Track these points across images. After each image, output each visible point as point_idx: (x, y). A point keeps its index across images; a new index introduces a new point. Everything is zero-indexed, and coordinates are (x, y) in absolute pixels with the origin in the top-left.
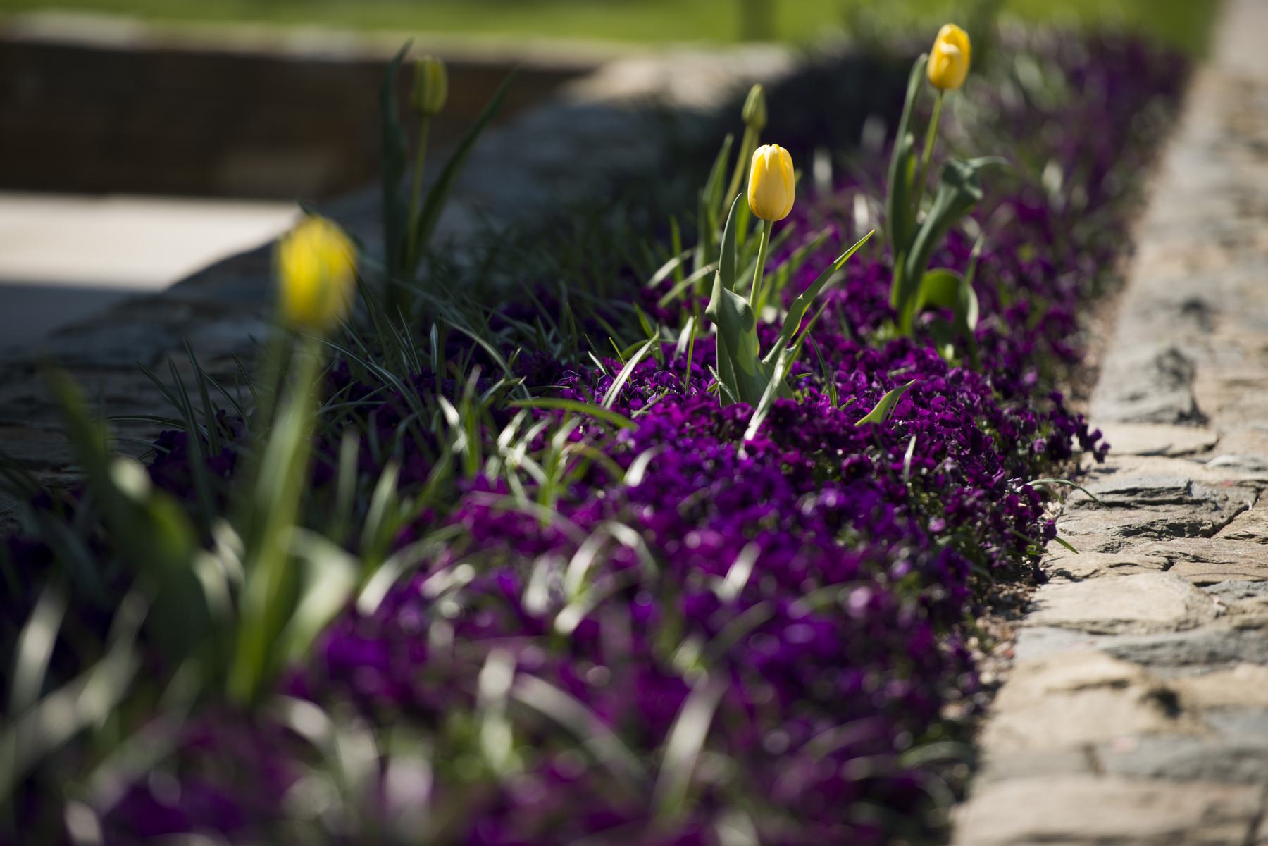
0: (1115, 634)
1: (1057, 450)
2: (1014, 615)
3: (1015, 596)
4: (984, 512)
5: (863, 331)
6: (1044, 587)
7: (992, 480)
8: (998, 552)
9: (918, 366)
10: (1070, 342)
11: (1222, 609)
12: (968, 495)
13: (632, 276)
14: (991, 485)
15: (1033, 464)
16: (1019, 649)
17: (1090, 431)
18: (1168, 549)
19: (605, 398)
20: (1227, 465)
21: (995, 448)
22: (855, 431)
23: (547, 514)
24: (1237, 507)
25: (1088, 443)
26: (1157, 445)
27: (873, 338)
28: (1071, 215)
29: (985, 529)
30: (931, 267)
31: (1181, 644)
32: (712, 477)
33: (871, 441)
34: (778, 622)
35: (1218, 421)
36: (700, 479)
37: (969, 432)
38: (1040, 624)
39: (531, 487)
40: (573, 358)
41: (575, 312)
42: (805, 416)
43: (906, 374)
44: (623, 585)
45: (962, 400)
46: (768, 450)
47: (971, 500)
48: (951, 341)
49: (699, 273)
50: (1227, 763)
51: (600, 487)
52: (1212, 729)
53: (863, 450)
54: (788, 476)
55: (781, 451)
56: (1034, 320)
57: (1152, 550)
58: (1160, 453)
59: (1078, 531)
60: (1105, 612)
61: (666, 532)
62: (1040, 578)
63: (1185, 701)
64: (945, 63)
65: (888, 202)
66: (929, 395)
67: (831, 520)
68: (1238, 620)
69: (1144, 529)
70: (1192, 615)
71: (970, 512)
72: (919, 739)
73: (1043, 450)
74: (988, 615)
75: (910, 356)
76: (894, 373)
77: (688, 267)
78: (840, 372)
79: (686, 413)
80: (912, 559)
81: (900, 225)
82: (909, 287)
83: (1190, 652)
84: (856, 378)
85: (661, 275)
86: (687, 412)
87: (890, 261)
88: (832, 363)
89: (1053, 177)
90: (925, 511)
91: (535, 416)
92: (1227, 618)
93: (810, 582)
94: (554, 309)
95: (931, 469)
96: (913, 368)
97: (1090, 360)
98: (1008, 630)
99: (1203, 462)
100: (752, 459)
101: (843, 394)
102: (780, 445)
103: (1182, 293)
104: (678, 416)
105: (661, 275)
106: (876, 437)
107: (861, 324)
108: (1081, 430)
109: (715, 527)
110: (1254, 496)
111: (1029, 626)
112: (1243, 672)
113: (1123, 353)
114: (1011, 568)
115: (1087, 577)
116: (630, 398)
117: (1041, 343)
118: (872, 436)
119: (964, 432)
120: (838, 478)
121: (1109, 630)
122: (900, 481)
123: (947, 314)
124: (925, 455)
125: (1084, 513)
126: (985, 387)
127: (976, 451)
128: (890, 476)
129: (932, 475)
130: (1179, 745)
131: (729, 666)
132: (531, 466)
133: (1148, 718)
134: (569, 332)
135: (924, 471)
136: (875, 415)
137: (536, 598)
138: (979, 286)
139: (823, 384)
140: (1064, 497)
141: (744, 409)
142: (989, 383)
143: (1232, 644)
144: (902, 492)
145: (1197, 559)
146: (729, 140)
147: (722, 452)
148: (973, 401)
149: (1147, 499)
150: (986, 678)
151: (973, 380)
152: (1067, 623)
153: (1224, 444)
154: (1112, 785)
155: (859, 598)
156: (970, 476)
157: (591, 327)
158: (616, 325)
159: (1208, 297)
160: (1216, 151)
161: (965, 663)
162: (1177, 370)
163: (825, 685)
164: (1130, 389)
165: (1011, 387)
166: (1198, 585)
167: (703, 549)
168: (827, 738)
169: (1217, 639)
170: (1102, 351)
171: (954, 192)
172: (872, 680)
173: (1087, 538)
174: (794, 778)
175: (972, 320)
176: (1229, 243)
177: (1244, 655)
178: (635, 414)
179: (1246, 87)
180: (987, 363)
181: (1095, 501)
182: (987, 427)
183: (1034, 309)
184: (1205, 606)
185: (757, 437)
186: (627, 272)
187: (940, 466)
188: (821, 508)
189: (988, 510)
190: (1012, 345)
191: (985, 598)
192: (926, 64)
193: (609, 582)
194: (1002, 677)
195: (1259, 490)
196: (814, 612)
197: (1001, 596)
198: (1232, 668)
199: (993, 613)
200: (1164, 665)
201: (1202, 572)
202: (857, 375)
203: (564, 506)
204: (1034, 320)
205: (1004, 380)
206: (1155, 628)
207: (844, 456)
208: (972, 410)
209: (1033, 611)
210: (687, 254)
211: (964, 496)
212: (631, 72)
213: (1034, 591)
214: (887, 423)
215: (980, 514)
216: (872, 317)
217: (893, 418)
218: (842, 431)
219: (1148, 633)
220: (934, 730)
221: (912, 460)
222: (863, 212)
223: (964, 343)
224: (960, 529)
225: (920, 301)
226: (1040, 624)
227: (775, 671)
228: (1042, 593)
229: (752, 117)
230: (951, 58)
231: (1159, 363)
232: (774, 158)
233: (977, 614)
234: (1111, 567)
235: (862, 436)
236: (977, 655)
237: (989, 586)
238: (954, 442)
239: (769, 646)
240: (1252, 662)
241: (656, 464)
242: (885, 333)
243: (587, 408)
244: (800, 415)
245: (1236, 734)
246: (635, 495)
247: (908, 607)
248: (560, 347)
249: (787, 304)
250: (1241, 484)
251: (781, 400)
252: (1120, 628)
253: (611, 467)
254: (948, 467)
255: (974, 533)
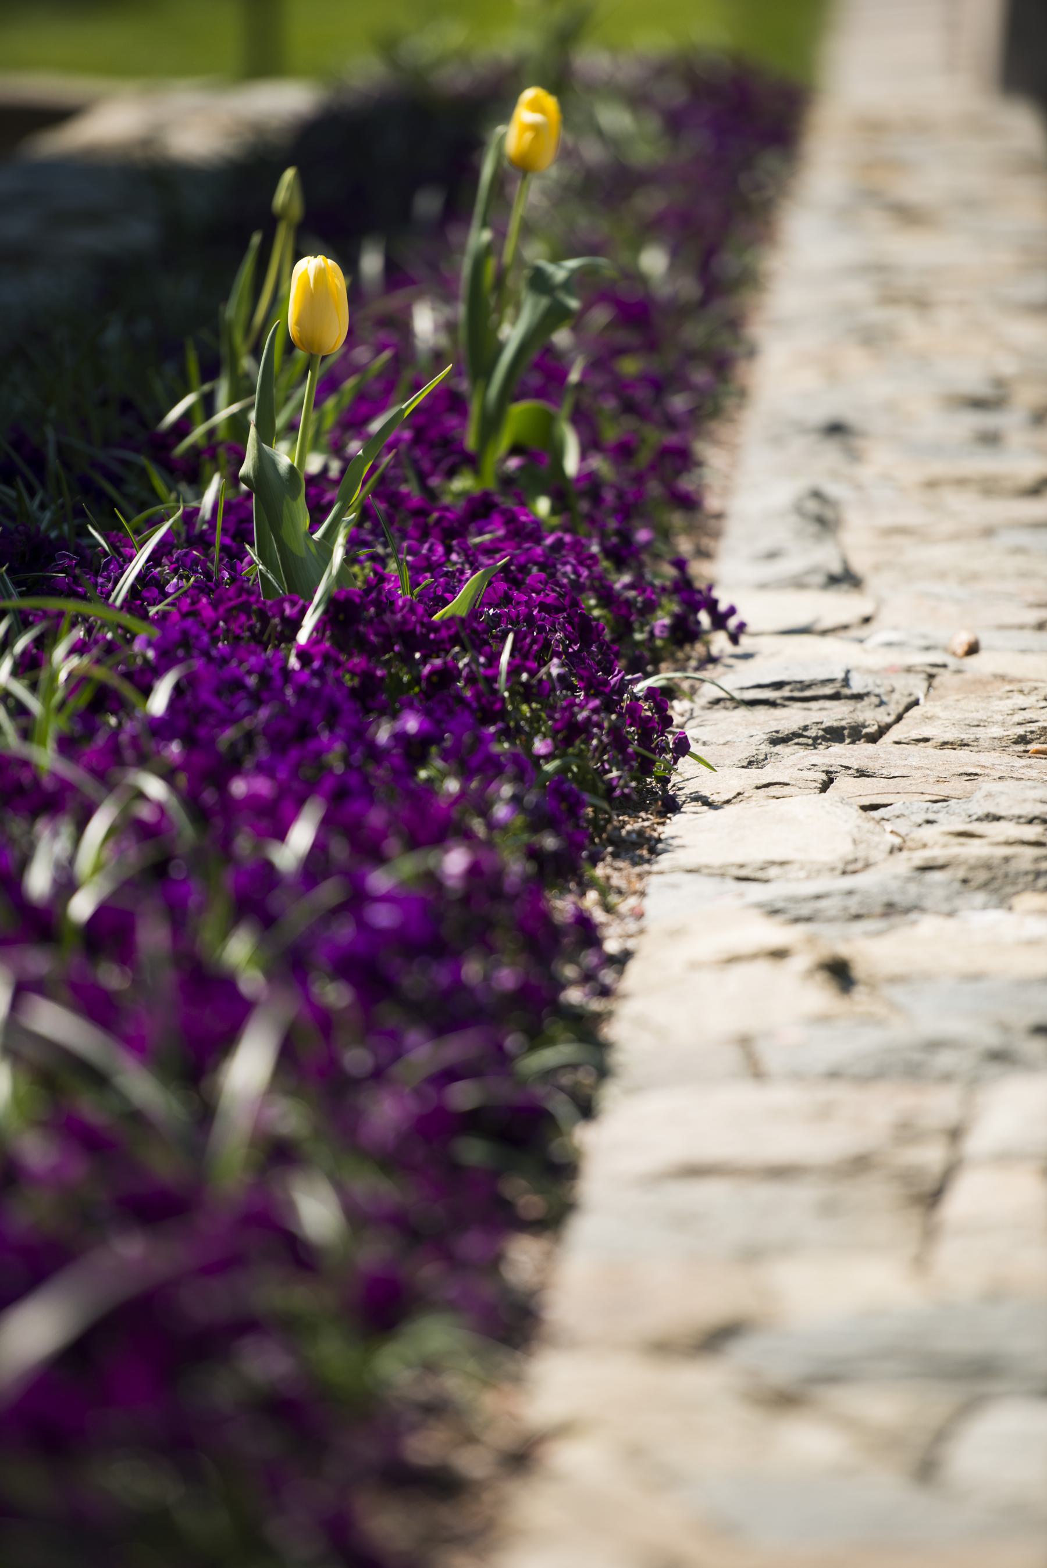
0: (766, 881)
1: (685, 633)
2: (641, 857)
3: (640, 833)
4: (600, 727)
5: (434, 482)
6: (677, 818)
7: (608, 682)
8: (620, 777)
9: (508, 532)
10: (686, 483)
11: (897, 841)
12: (582, 707)
13: (137, 413)
14: (607, 690)
15: (654, 650)
16: (649, 905)
17: (722, 607)
18: (827, 761)
19: (114, 594)
20: (890, 644)
21: (607, 635)
22: (435, 627)
23: (46, 757)
24: (906, 701)
25: (720, 621)
26: (801, 619)
27: (444, 492)
28: (682, 311)
29: (602, 749)
30: (517, 399)
31: (850, 893)
32: (257, 699)
33: (455, 640)
34: (358, 898)
35: (874, 583)
36: (243, 706)
37: (576, 620)
38: (673, 870)
39: (23, 721)
40: (66, 528)
41: (66, 465)
42: (372, 610)
43: (492, 541)
44: (154, 866)
45: (565, 574)
46: (327, 658)
47: (584, 714)
48: (545, 492)
49: (224, 413)
50: (917, 1056)
51: (114, 713)
52: (894, 1007)
53: (448, 652)
54: (353, 689)
55: (343, 657)
56: (644, 457)
57: (807, 763)
58: (804, 631)
59: (715, 735)
60: (752, 852)
61: (203, 777)
62: (671, 806)
63: (859, 971)
64: (529, 136)
65: (461, 310)
66: (523, 569)
67: (413, 750)
68: (920, 857)
69: (796, 735)
70: (861, 853)
71: (583, 730)
72: (537, 1039)
73: (666, 634)
74: (609, 859)
75: (496, 517)
76: (478, 540)
77: (208, 405)
78: (411, 542)
79: (220, 613)
80: (516, 800)
81: (476, 344)
82: (491, 424)
83: (861, 903)
84: (431, 549)
85: (175, 414)
86: (221, 610)
87: (464, 386)
88: (400, 530)
89: (654, 261)
90: (527, 729)
91: (23, 622)
92: (904, 854)
93: (393, 845)
94: (37, 462)
95: (532, 674)
96: (501, 533)
97: (712, 503)
98: (634, 879)
99: (861, 641)
100: (307, 671)
101: (416, 571)
102: (342, 649)
103: (821, 412)
104: (208, 613)
105: (175, 414)
106: (463, 634)
107: (432, 473)
108: (711, 605)
109: (262, 769)
110: (925, 684)
111: (661, 873)
112: (927, 926)
113: (752, 488)
114: (635, 797)
115: (728, 802)
116: (144, 586)
117: (654, 488)
118: (457, 634)
119: (569, 620)
120: (417, 689)
121: (759, 875)
122: (495, 692)
123: (539, 455)
124: (525, 657)
125: (719, 714)
126: (593, 557)
127: (586, 645)
128: (482, 685)
129: (534, 682)
130: (855, 1032)
131: (292, 966)
132: (19, 689)
133: (820, 996)
134: (60, 494)
135: (525, 676)
136: (458, 606)
137: (39, 881)
138: (581, 419)
139: (388, 556)
140: (693, 691)
141: (294, 604)
142: (595, 549)
143: (913, 889)
144: (498, 706)
145: (862, 774)
146: (256, 239)
147: (268, 662)
148: (579, 575)
149: (796, 694)
150: (611, 946)
151: (578, 547)
152: (707, 867)
153: (886, 617)
154: (781, 1095)
155: (455, 862)
156: (581, 679)
157: (86, 486)
158: (117, 481)
159: (850, 415)
160: (845, 216)
161: (587, 932)
162: (822, 517)
163: (417, 979)
164: (765, 543)
165: (623, 554)
166: (865, 808)
167: (252, 800)
168: (423, 1054)
169: (894, 885)
170: (726, 492)
171: (544, 302)
172: (473, 970)
173: (726, 749)
174: (386, 1113)
175: (571, 464)
176: (872, 339)
177: (928, 903)
178: (153, 611)
179: (873, 127)
180: (591, 520)
181: (732, 699)
182: (596, 606)
183: (643, 441)
184: (876, 839)
185: (312, 641)
186: (127, 406)
187: (544, 670)
188: (400, 737)
189: (606, 724)
190: (621, 495)
191: (604, 836)
192: (503, 138)
193: (135, 855)
194: (630, 944)
195: (931, 677)
196: (402, 884)
197: (624, 832)
198: (914, 923)
199: (615, 856)
200: (831, 920)
201: (870, 790)
202: (432, 545)
203: (66, 745)
204: (644, 457)
205: (615, 546)
206: (815, 871)
207: (424, 661)
208: (578, 587)
209: (665, 851)
210: (206, 387)
211: (576, 709)
212: (113, 121)
213: (663, 824)
214: (474, 613)
215: (595, 730)
216: (445, 465)
217: (482, 605)
218: (419, 629)
219: (808, 877)
220: (555, 1027)
221: (509, 664)
222: (425, 322)
223: (561, 494)
224: (571, 750)
225: (505, 441)
226: (673, 870)
227: (352, 967)
228: (674, 827)
229: (286, 207)
230: (536, 128)
231: (799, 510)
232: (321, 273)
233: (595, 859)
234: (758, 788)
235: (444, 633)
236: (599, 916)
237: (609, 821)
238: (559, 635)
239: (344, 931)
240: (938, 913)
241: (184, 683)
242: (463, 483)
243: (94, 610)
244: (368, 610)
245: (930, 1017)
246: (161, 729)
247: (516, 867)
248: (48, 515)
249: (337, 449)
250: (909, 670)
251: (341, 590)
252: (773, 872)
253: (128, 691)
254: (555, 671)
255: (590, 755)
